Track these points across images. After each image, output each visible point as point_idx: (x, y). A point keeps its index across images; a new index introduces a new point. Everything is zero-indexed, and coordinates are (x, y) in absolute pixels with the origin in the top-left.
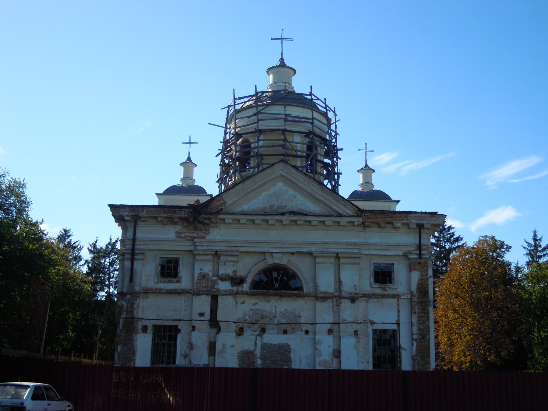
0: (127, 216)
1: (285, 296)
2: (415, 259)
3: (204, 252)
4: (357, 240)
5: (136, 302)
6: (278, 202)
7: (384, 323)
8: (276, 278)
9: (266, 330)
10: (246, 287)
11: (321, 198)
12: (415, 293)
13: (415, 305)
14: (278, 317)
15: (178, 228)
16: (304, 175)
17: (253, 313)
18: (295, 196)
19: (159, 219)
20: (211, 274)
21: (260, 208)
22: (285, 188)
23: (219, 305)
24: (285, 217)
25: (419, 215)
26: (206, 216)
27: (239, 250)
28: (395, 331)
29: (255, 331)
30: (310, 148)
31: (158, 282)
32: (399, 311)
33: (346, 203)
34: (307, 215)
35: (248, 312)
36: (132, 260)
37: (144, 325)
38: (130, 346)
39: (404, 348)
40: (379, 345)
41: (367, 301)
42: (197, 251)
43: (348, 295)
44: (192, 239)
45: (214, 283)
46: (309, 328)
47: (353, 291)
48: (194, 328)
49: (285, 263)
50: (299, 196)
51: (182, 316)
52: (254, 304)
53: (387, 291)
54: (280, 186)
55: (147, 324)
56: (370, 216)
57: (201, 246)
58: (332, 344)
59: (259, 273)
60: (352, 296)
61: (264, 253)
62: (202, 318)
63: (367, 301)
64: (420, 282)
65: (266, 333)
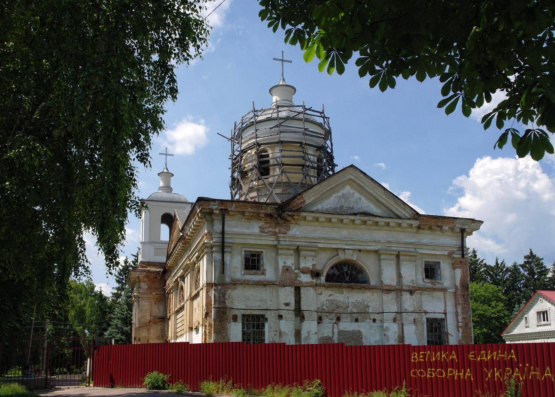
0: (216, 209)
1: (355, 288)
2: (459, 258)
3: (288, 247)
4: (413, 241)
5: (227, 293)
6: (347, 204)
7: (435, 313)
8: (347, 273)
9: (341, 318)
10: (323, 279)
11: (384, 202)
12: (459, 287)
13: (459, 298)
14: (350, 307)
15: (261, 224)
16: (371, 180)
17: (329, 303)
18: (360, 199)
19: (247, 214)
20: (293, 268)
21: (332, 208)
22: (352, 191)
23: (302, 295)
24: (357, 217)
25: (462, 221)
26: (290, 213)
27: (317, 246)
28: (443, 319)
29: (332, 319)
30: (319, 160)
31: (245, 274)
32: (445, 303)
33: (406, 207)
34: (375, 216)
35: (325, 303)
36: (223, 252)
37: (234, 314)
38: (225, 334)
39: (451, 334)
40: (431, 331)
41: (421, 294)
42: (281, 245)
43: (408, 289)
44: (275, 234)
45: (297, 275)
46: (377, 317)
47: (411, 284)
48: (280, 317)
49: (355, 259)
50: (363, 199)
51: (269, 306)
52: (330, 296)
53: (436, 285)
54: (348, 189)
55: (236, 314)
56: (425, 220)
57: (284, 241)
58: (397, 331)
59: (332, 268)
60: (411, 289)
61: (337, 249)
62: (287, 308)
63: (421, 294)
64: (462, 278)
65: (341, 321)
